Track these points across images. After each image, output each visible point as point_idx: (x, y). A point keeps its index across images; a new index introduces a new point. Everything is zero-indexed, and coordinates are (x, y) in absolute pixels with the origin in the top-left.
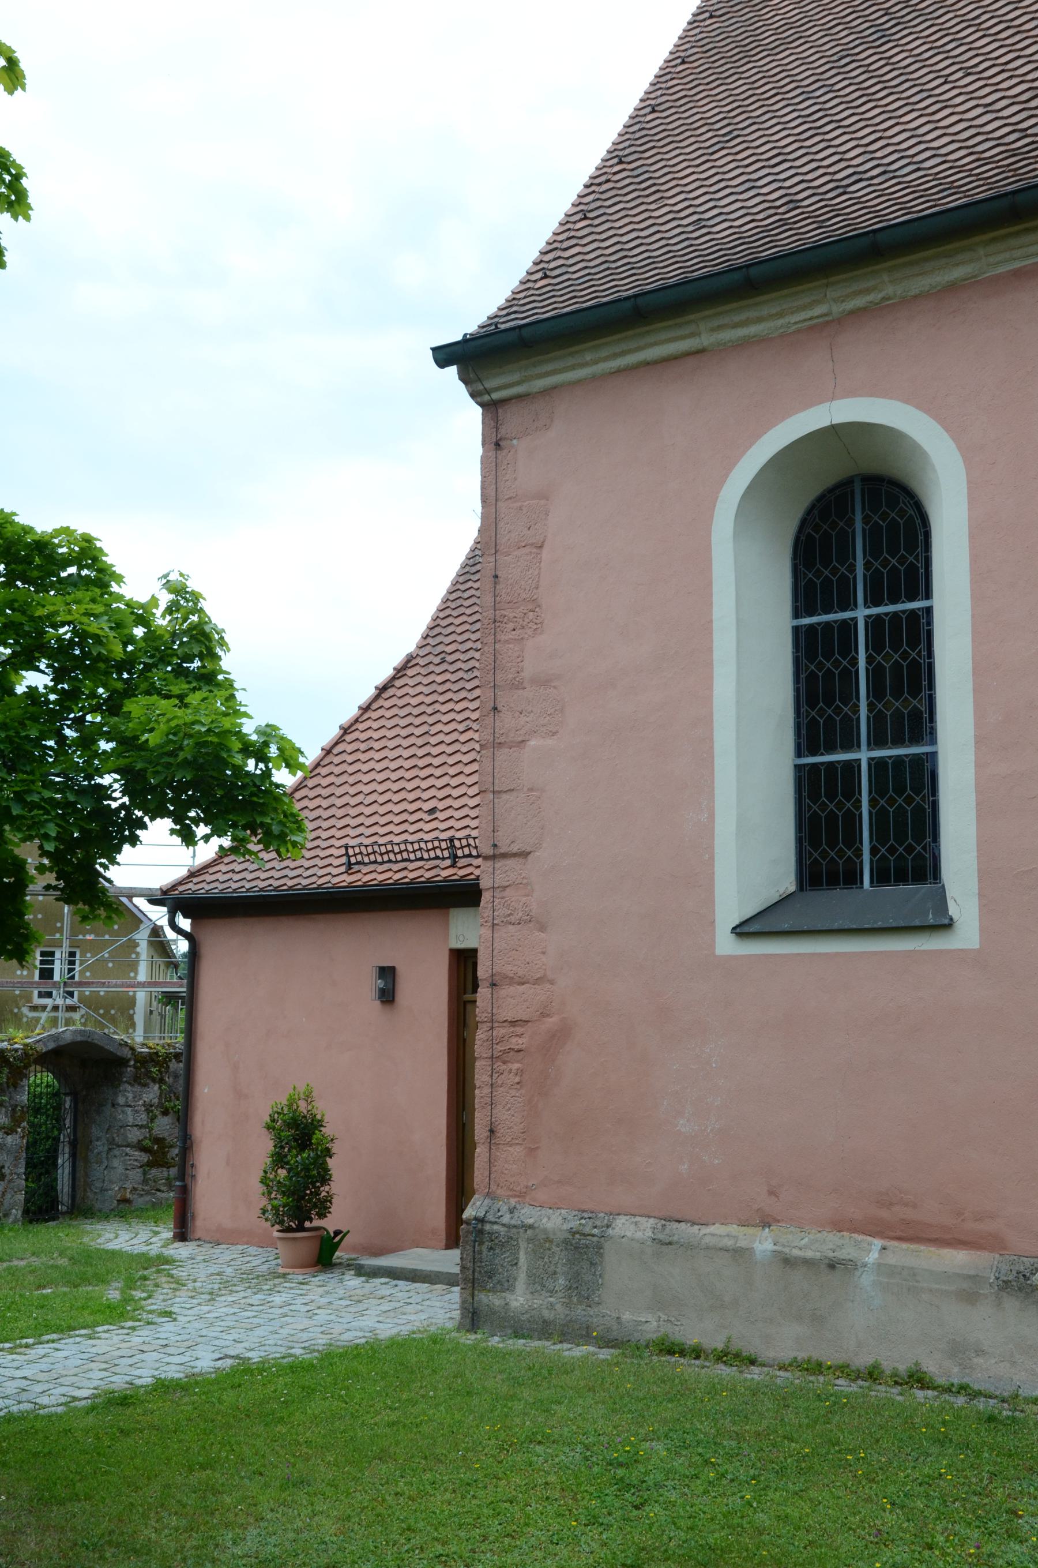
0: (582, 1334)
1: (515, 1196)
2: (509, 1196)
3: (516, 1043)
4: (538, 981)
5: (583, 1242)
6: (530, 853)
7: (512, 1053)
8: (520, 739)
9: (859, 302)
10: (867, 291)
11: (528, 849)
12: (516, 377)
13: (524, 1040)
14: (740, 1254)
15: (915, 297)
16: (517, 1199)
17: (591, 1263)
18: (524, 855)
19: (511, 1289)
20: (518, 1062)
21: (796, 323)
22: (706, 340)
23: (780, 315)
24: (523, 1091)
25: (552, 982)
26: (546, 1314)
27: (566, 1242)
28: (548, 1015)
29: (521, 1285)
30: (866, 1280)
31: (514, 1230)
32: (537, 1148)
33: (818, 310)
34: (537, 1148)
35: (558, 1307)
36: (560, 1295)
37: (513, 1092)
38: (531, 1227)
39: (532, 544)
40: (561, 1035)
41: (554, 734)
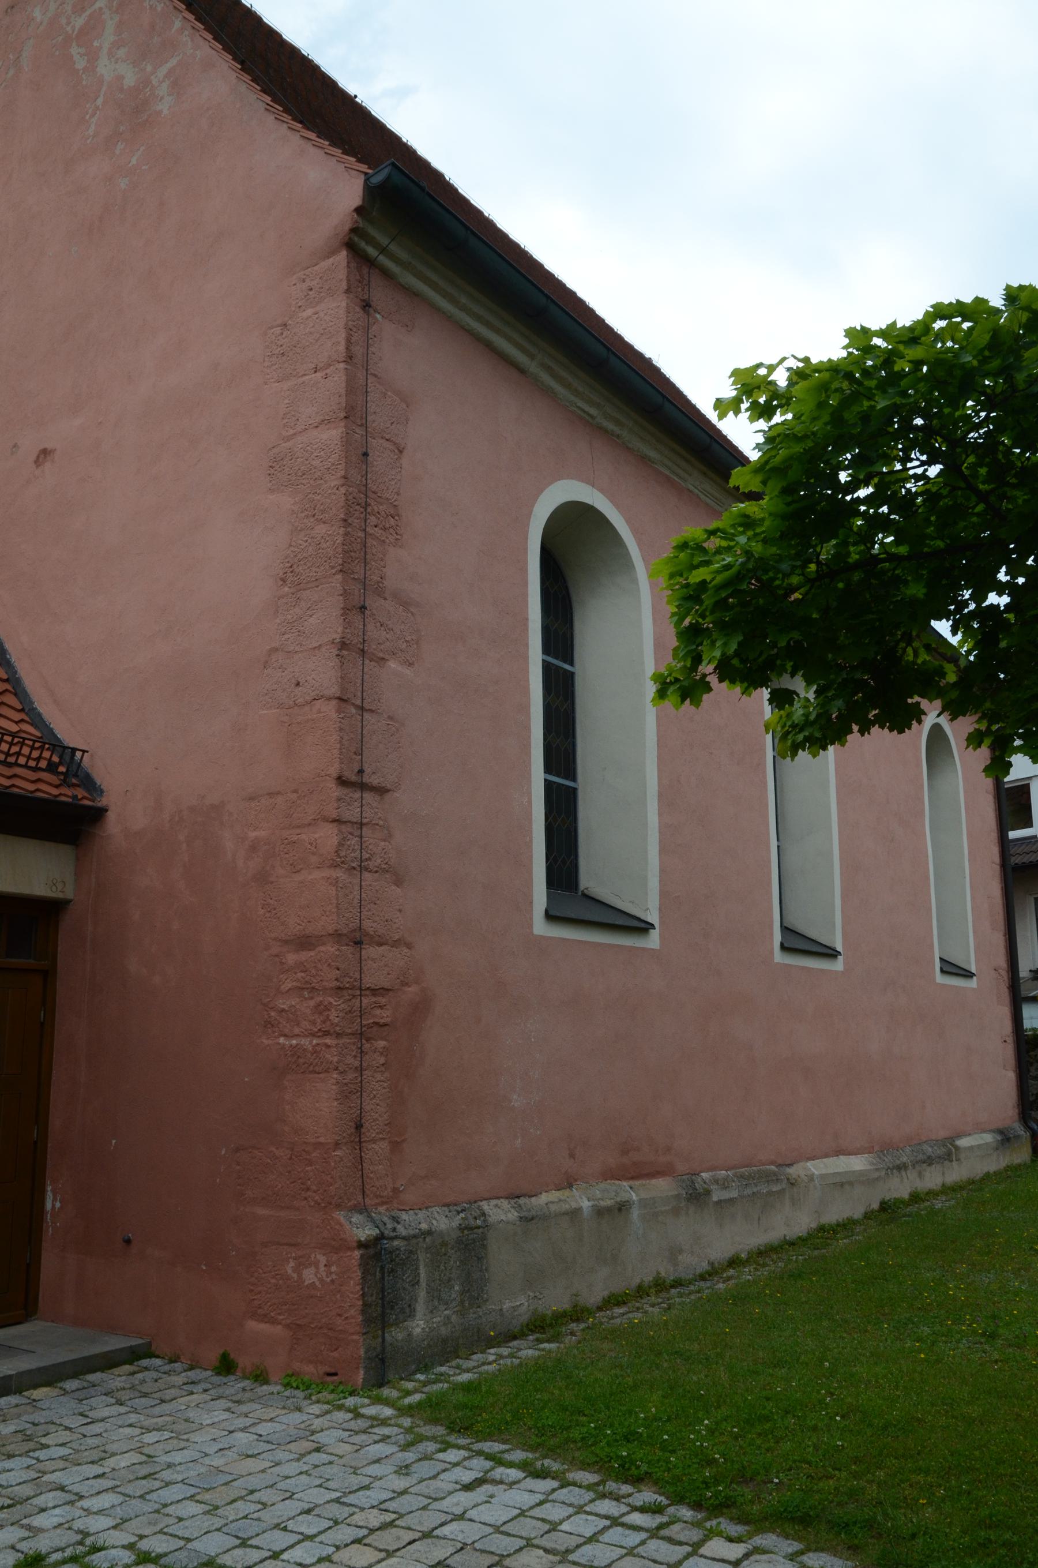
0: (481, 1340)
1: (383, 1203)
2: (377, 1204)
3: (384, 1015)
4: (396, 944)
5: (471, 1237)
6: (388, 791)
7: (375, 1029)
8: (381, 655)
9: (610, 426)
10: (617, 422)
11: (389, 786)
12: (403, 255)
13: (388, 1013)
14: (574, 1214)
15: (627, 448)
16: (385, 1207)
17: (479, 1259)
18: (381, 791)
19: (412, 1314)
20: (382, 1039)
21: (578, 407)
22: (533, 367)
23: (576, 393)
24: (387, 1074)
25: (409, 946)
26: (443, 1331)
27: (459, 1241)
28: (407, 984)
29: (420, 1308)
30: (635, 1213)
31: (414, 1241)
32: (403, 1141)
33: (593, 411)
34: (403, 1141)
35: (454, 1318)
36: (454, 1304)
37: (379, 1077)
38: (429, 1232)
39: (395, 444)
40: (421, 1008)
41: (411, 664)
